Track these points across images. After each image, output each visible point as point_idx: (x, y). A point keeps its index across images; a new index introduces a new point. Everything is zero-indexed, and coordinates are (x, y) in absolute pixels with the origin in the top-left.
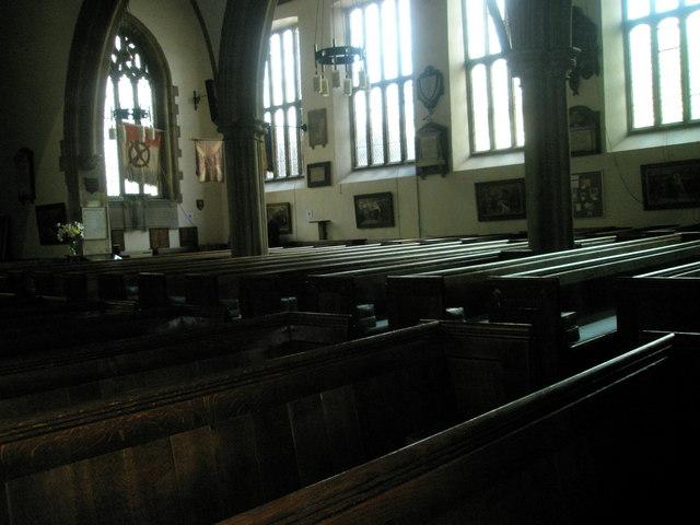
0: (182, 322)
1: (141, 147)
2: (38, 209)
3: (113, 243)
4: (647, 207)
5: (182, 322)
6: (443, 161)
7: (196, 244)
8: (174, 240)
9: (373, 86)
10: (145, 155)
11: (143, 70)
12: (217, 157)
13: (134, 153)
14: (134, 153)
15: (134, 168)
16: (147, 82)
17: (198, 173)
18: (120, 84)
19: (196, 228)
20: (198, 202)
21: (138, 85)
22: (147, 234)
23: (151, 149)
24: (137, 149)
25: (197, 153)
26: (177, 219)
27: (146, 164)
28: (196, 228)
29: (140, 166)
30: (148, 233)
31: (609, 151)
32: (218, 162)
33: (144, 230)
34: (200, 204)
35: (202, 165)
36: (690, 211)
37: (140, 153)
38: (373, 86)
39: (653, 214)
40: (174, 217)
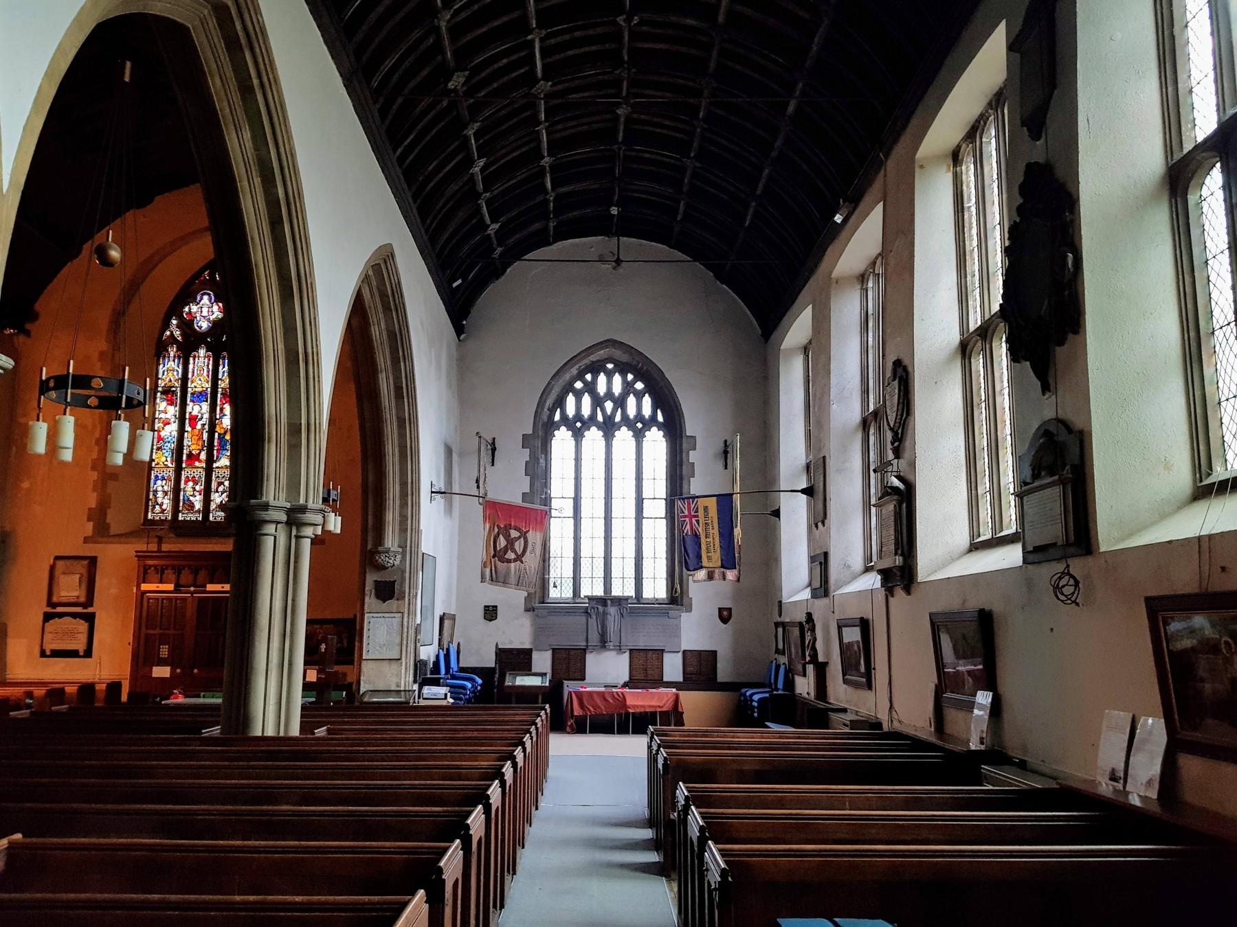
1: (514, 534)
6: (899, 561)
8: (673, 668)
10: (519, 546)
11: (654, 417)
13: (502, 542)
14: (502, 542)
16: (661, 433)
18: (615, 442)
21: (584, 442)
22: (626, 657)
23: (530, 535)
24: (507, 537)
26: (679, 637)
27: (519, 558)
29: (509, 561)
30: (627, 655)
31: (1102, 549)
33: (619, 649)
34: (725, 616)
36: (1156, 769)
37: (511, 543)
40: (676, 632)
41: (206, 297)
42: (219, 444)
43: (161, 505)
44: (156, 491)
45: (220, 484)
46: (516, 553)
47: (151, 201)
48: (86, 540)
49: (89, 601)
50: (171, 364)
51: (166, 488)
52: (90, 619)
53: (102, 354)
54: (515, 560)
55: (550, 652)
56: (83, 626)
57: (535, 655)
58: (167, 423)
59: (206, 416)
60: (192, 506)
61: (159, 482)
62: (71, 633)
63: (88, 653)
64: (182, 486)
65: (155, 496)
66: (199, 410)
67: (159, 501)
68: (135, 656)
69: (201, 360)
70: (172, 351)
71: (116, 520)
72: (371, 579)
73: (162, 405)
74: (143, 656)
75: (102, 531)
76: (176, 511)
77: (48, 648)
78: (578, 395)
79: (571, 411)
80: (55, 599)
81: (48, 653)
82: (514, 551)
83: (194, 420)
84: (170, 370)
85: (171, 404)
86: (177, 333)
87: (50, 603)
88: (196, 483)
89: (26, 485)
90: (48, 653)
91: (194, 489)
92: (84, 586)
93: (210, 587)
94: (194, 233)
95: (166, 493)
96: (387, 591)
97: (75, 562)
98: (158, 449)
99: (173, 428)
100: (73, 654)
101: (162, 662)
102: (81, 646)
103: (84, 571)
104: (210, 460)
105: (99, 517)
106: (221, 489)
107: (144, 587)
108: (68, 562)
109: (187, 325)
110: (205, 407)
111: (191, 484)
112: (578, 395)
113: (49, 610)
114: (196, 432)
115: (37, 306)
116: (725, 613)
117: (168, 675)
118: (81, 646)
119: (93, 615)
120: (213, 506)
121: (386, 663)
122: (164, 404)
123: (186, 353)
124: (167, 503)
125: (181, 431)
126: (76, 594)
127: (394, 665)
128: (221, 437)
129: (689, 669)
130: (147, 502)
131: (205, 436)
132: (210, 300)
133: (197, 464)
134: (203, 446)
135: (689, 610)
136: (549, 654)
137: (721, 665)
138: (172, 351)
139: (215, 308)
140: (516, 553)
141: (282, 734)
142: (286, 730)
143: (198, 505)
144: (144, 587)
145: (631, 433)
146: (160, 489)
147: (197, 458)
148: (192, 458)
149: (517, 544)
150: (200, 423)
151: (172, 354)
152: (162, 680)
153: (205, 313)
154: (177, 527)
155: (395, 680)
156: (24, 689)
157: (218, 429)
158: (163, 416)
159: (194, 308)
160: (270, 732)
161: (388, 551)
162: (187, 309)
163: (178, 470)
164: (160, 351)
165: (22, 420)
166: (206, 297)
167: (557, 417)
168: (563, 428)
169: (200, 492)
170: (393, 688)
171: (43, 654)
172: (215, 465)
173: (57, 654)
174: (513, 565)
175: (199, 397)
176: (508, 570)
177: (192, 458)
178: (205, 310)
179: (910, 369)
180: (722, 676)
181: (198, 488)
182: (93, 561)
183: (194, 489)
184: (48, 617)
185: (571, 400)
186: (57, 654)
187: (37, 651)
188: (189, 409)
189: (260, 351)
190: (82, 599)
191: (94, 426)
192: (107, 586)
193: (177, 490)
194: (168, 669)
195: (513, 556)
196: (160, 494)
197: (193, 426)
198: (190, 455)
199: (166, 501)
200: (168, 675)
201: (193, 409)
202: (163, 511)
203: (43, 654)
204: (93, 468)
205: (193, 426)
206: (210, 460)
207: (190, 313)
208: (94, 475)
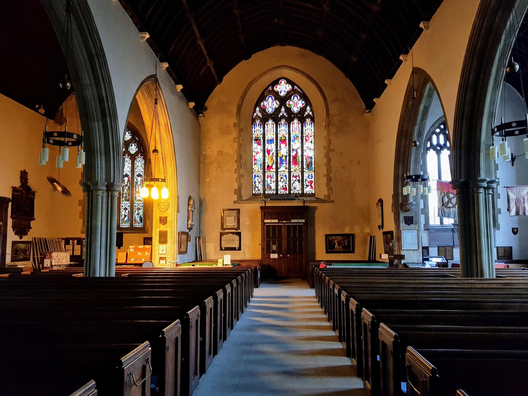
0: (21, 238)
3: (423, 256)
5: (21, 238)
9: (442, 222)
11: (445, 145)
14: (446, 200)
17: (509, 210)
19: (511, 248)
20: (513, 229)
21: (441, 155)
24: (448, 197)
28: (511, 248)
29: (449, 208)
34: (515, 231)
38: (442, 222)
41: (270, 98)
42: (280, 161)
43: (258, 188)
44: (255, 182)
45: (282, 178)
46: (453, 204)
47: (250, 57)
48: (235, 202)
50: (258, 128)
51: (259, 180)
52: (239, 234)
53: (235, 124)
54: (452, 207)
55: (437, 248)
56: (237, 237)
57: (430, 249)
58: (258, 153)
59: (274, 149)
60: (271, 188)
61: (256, 178)
62: (231, 240)
63: (240, 249)
65: (255, 184)
66: (271, 147)
69: (270, 125)
70: (258, 122)
71: (245, 195)
72: (402, 215)
73: (255, 145)
74: (266, 250)
75: (240, 199)
76: (264, 190)
77: (223, 246)
78: (438, 135)
79: (435, 142)
80: (225, 227)
83: (269, 151)
84: (257, 131)
85: (259, 145)
86: (259, 114)
87: (223, 228)
89: (208, 180)
93: (293, 221)
94: (268, 71)
96: (409, 221)
97: (231, 212)
99: (261, 155)
100: (234, 249)
101: (274, 252)
102: (237, 246)
103: (236, 215)
104: (277, 168)
105: (238, 192)
106: (282, 180)
108: (229, 212)
109: (263, 110)
111: (269, 178)
112: (438, 135)
113: (222, 231)
114: (270, 156)
115: (206, 104)
116: (515, 230)
118: (237, 246)
119: (240, 233)
120: (279, 188)
122: (256, 144)
124: (260, 187)
126: (233, 224)
127: (416, 252)
128: (281, 158)
129: (500, 255)
130: (252, 186)
131: (274, 158)
133: (271, 170)
135: (499, 229)
136: (436, 249)
138: (258, 122)
139: (275, 102)
140: (453, 204)
142: (492, 276)
144: (266, 221)
145: (435, 152)
146: (257, 181)
147: (271, 167)
148: (269, 167)
151: (308, 122)
152: (275, 259)
153: (270, 105)
154: (276, 197)
156: (247, 264)
158: (256, 150)
159: (265, 103)
161: (411, 203)
162: (262, 104)
163: (264, 173)
164: (253, 121)
165: (204, 153)
166: (270, 98)
169: (274, 182)
170: (416, 262)
171: (221, 249)
173: (227, 249)
174: (452, 209)
176: (450, 211)
177: (269, 167)
179: (144, 137)
180: (515, 257)
181: (272, 180)
182: (238, 210)
183: (271, 181)
184: (221, 235)
185: (434, 137)
186: (227, 249)
188: (266, 147)
190: (236, 227)
191: (234, 154)
193: (264, 181)
195: (451, 205)
196: (257, 183)
197: (269, 154)
198: (268, 166)
201: (268, 146)
202: (259, 190)
203: (221, 249)
204: (235, 173)
205: (269, 154)
206: (277, 168)
207: (264, 105)
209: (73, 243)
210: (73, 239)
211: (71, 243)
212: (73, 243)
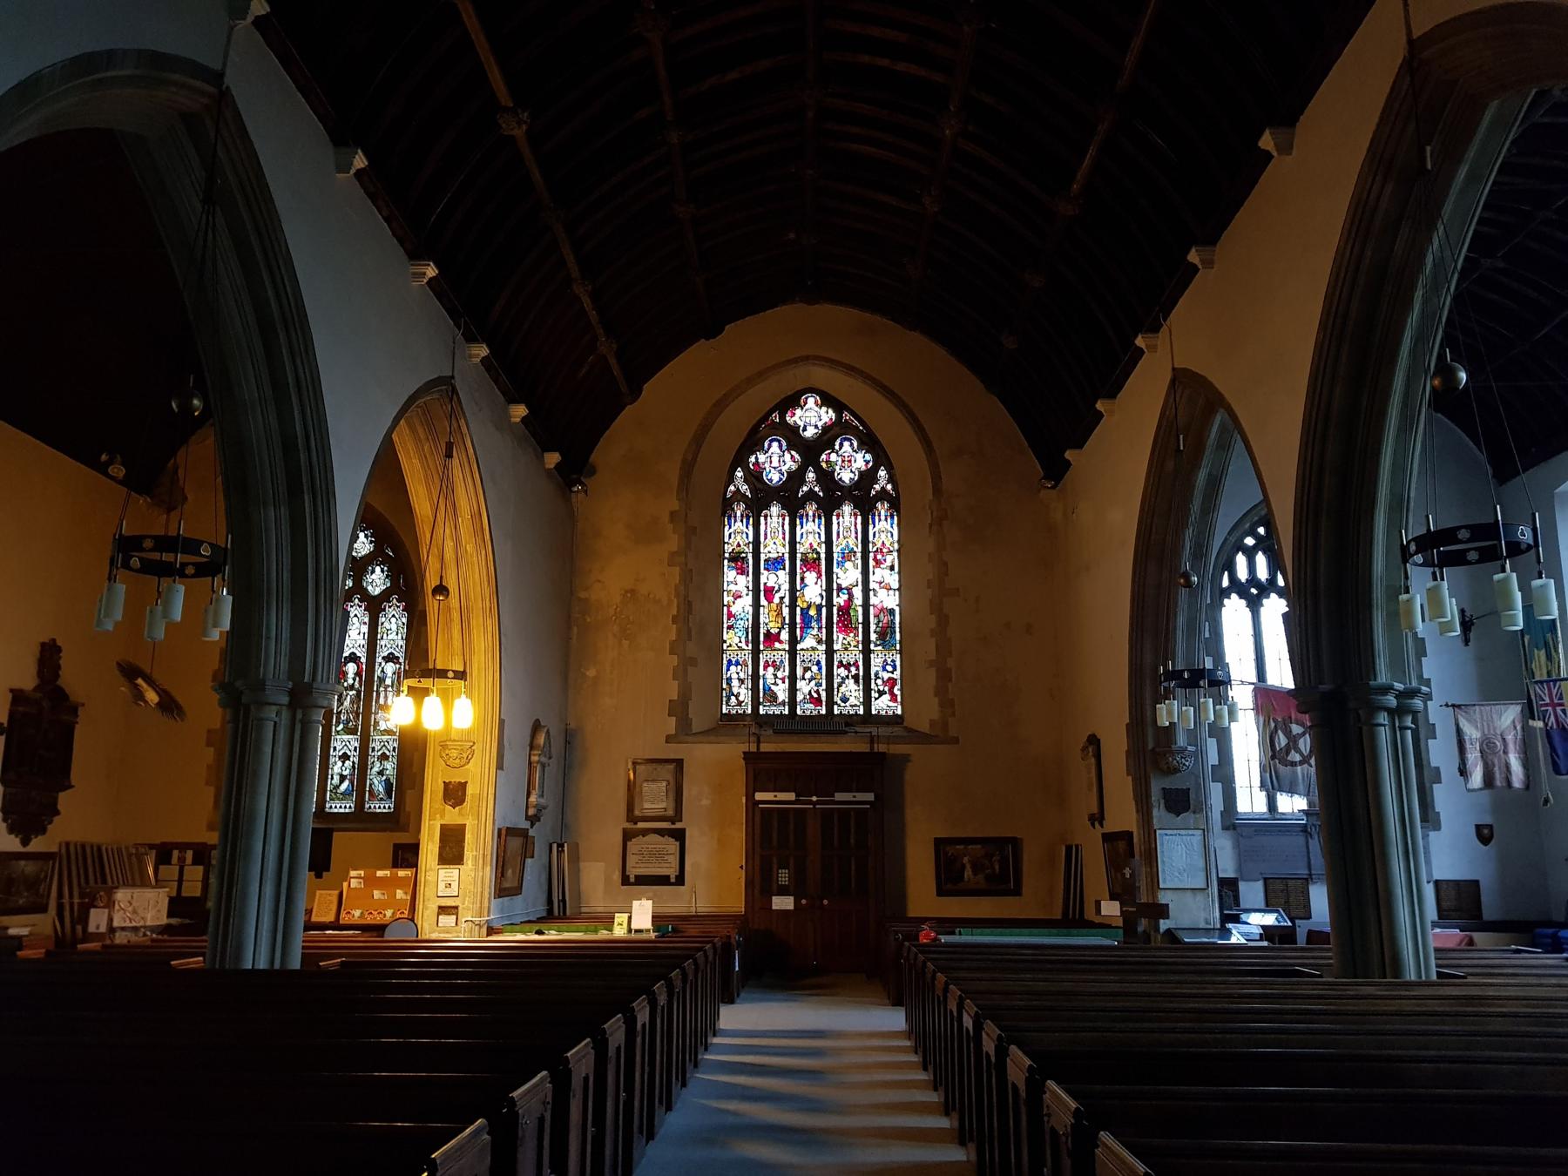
2: (1107, 837)
4: (941, 892)
5: (25, 843)
7: (1480, 916)
11: (1272, 580)
12: (1510, 738)
13: (1282, 740)
14: (1282, 740)
15: (1281, 768)
17: (1463, 771)
20: (1478, 827)
24: (1288, 733)
25: (1459, 732)
29: (1293, 764)
32: (1511, 747)
34: (1484, 834)
35: (1473, 756)
39: (469, 854)
41: (775, 444)
42: (803, 620)
44: (729, 680)
45: (806, 669)
46: (1301, 754)
48: (669, 739)
49: (678, 816)
50: (811, 526)
51: (742, 675)
52: (679, 836)
53: (672, 514)
54: (1301, 763)
56: (672, 846)
57: (1242, 886)
58: (737, 596)
59: (786, 586)
61: (733, 668)
63: (680, 880)
64: (762, 672)
66: (777, 580)
67: (735, 691)
68: (749, 884)
70: (739, 510)
73: (730, 574)
74: (760, 885)
75: (684, 731)
76: (756, 703)
77: (632, 872)
79: (1242, 574)
80: (637, 813)
81: (632, 880)
82: (1298, 751)
83: (770, 592)
84: (737, 534)
86: (744, 488)
87: (631, 817)
88: (777, 668)
89: (591, 673)
90: (632, 880)
91: (776, 676)
92: (672, 796)
93: (839, 796)
95: (742, 681)
97: (659, 767)
98: (730, 627)
99: (747, 600)
100: (663, 880)
101: (783, 892)
102: (672, 872)
103: (670, 777)
104: (793, 641)
105: (679, 709)
106: (808, 675)
107: (759, 796)
109: (755, 477)
110: (783, 576)
111: (771, 670)
114: (774, 606)
115: (593, 458)
117: (791, 907)
118: (672, 872)
119: (683, 831)
120: (800, 697)
121: (1189, 893)
123: (828, 509)
124: (745, 694)
125: (756, 605)
126: (663, 805)
127: (1200, 897)
130: (717, 688)
131: (786, 611)
132: (780, 447)
133: (777, 645)
134: (783, 623)
136: (1260, 885)
137: (1485, 898)
138: (739, 510)
139: (787, 457)
140: (1301, 754)
141: (277, 966)
143: (782, 695)
144: (759, 796)
146: (735, 676)
147: (777, 637)
148: (772, 638)
149: (1301, 743)
150: (777, 596)
152: (784, 913)
153: (775, 464)
155: (1203, 915)
157: (799, 602)
158: (732, 587)
159: (762, 458)
160: (262, 964)
162: (753, 459)
163: (756, 653)
164: (726, 508)
165: (583, 595)
166: (775, 444)
167: (1225, 583)
168: (1234, 596)
171: (625, 881)
172: (799, 647)
175: (775, 564)
176: (1295, 773)
177: (772, 638)
178: (775, 460)
180: (1489, 913)
181: (780, 674)
182: (679, 763)
183: (776, 676)
184: (627, 836)
185: (1241, 560)
187: (617, 876)
188: (763, 579)
189: (1375, 493)
190: (671, 812)
192: (697, 795)
193: (755, 677)
194: (792, 899)
195: (1298, 758)
196: (735, 683)
198: (768, 634)
199: (743, 691)
200: (791, 907)
202: (740, 703)
203: (625, 881)
206: (793, 641)
207: (757, 463)
208: (674, 660)
209: (182, 860)
210: (183, 847)
211: (175, 859)
212: (182, 860)
